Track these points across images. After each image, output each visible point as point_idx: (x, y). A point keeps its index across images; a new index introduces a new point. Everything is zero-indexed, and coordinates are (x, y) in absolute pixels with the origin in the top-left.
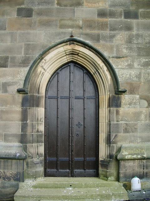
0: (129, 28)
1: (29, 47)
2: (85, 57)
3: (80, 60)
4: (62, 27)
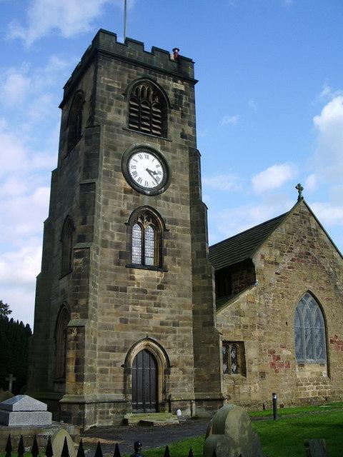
0: (175, 332)
1: (127, 342)
2: (153, 348)
3: (150, 349)
4: (143, 330)
